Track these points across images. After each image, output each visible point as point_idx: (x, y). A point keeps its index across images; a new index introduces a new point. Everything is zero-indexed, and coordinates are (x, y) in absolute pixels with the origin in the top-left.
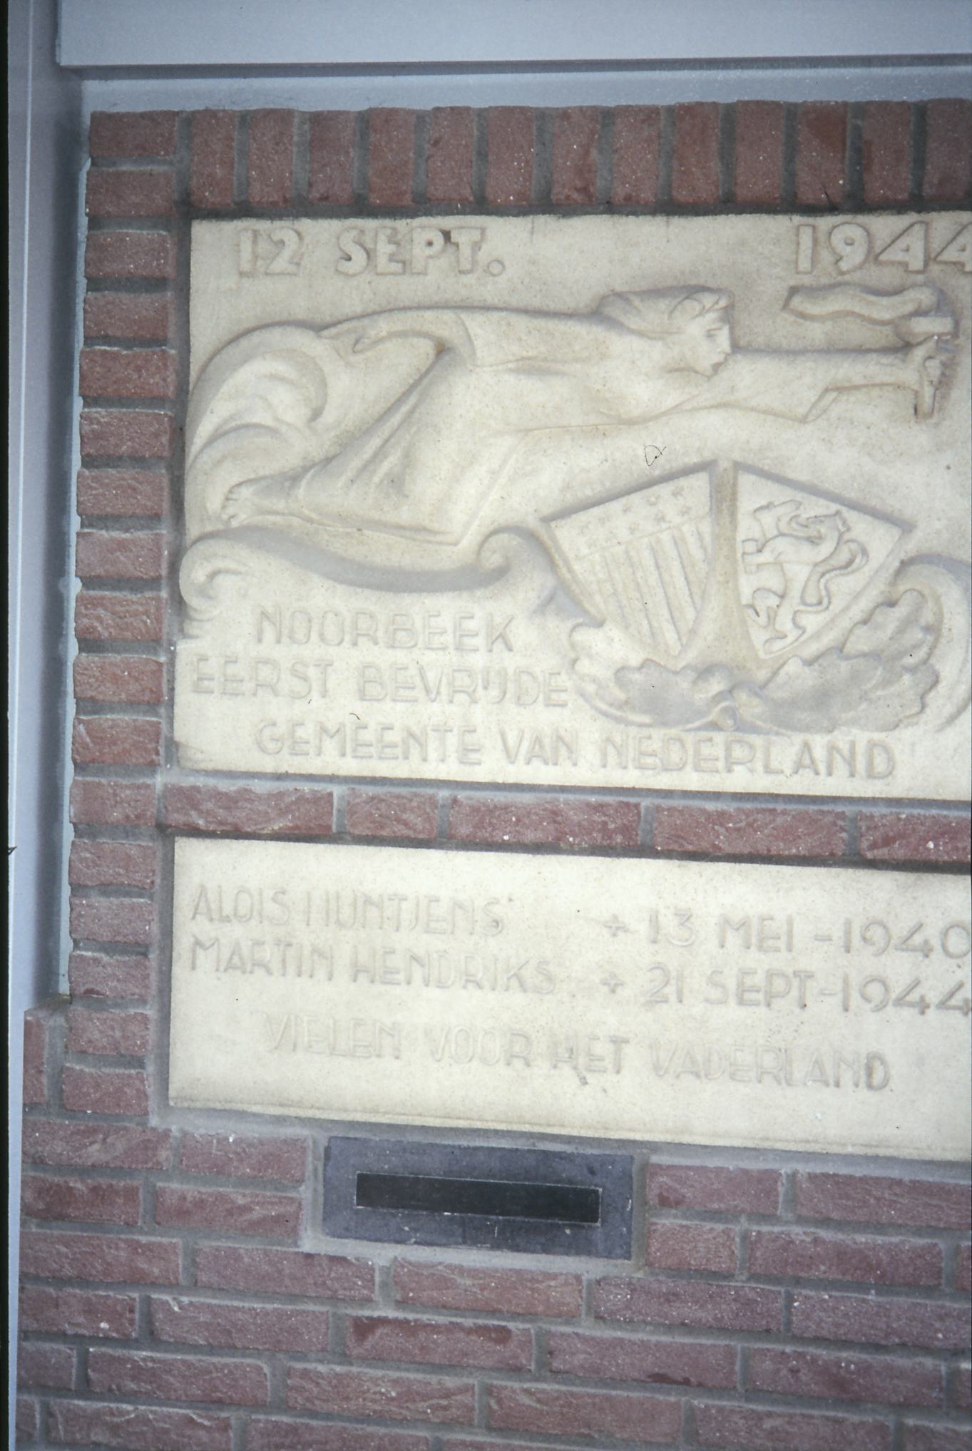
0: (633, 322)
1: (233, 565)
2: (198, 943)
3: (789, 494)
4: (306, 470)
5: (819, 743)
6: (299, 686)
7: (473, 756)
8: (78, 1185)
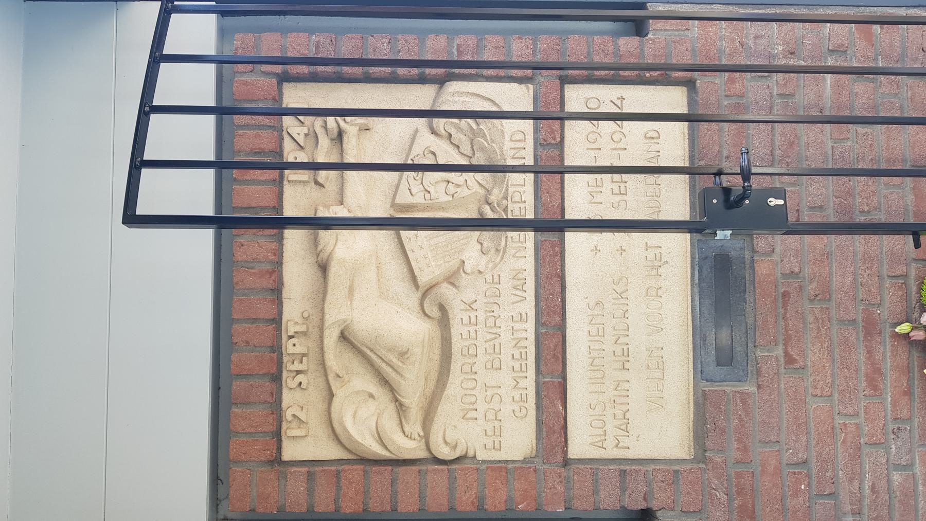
0: (329, 249)
1: (441, 434)
2: (617, 446)
4: (397, 400)
6: (496, 398)
7: (524, 316)
8: (736, 503)
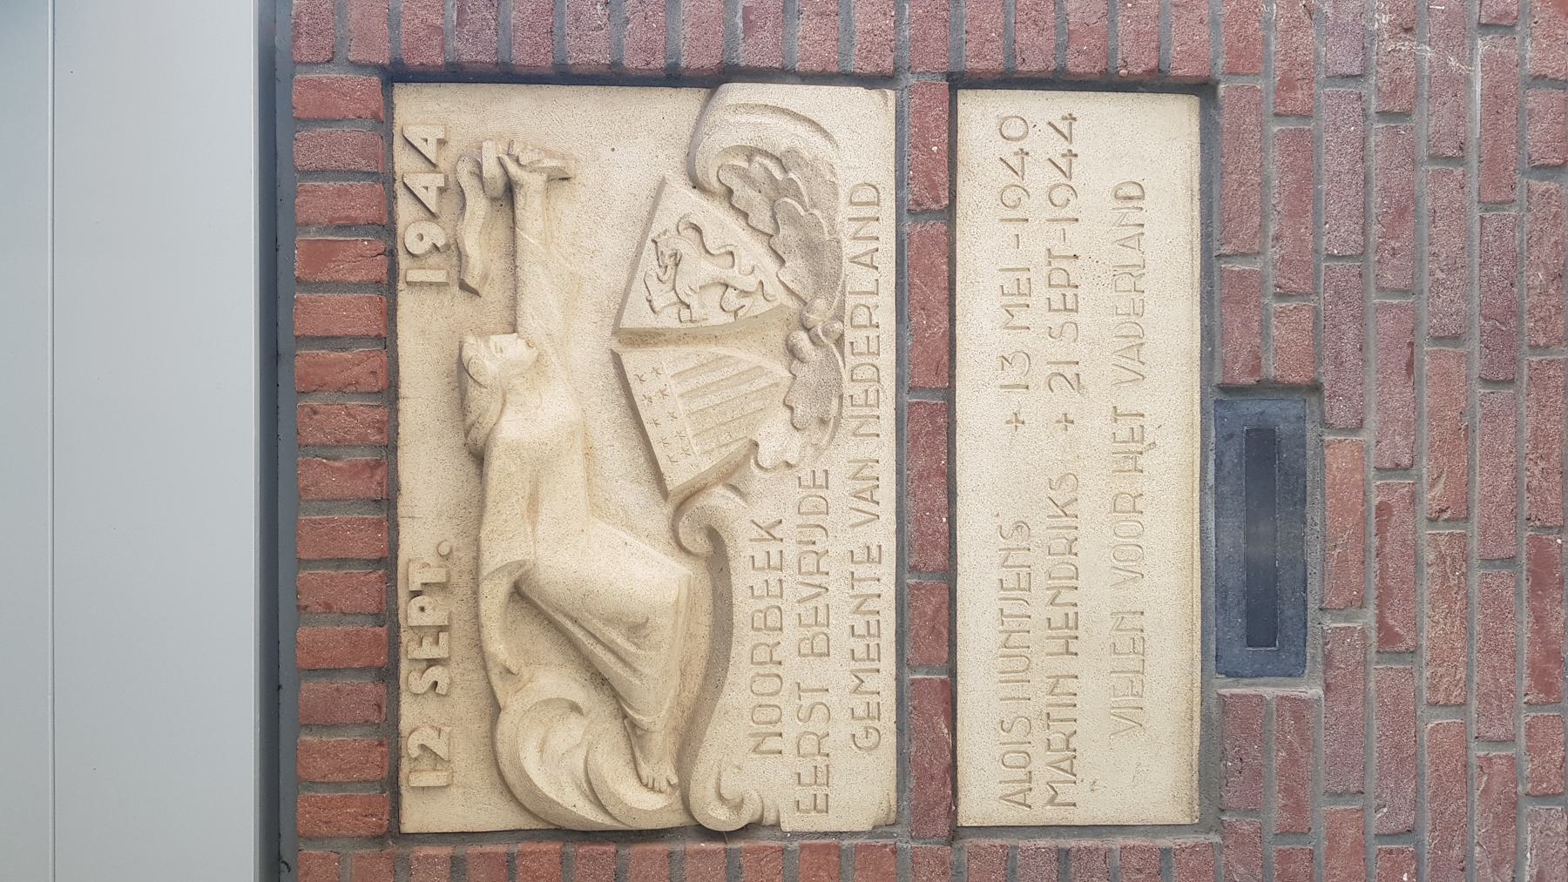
0: (488, 420)
2: (1052, 801)
3: (638, 285)
5: (850, 249)
6: (820, 712)
7: (875, 552)
